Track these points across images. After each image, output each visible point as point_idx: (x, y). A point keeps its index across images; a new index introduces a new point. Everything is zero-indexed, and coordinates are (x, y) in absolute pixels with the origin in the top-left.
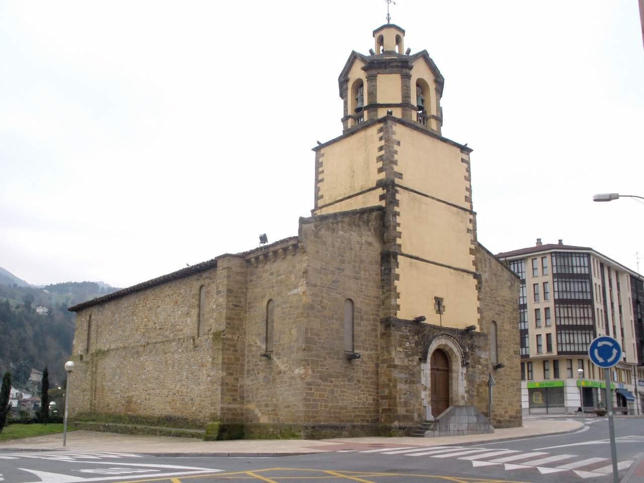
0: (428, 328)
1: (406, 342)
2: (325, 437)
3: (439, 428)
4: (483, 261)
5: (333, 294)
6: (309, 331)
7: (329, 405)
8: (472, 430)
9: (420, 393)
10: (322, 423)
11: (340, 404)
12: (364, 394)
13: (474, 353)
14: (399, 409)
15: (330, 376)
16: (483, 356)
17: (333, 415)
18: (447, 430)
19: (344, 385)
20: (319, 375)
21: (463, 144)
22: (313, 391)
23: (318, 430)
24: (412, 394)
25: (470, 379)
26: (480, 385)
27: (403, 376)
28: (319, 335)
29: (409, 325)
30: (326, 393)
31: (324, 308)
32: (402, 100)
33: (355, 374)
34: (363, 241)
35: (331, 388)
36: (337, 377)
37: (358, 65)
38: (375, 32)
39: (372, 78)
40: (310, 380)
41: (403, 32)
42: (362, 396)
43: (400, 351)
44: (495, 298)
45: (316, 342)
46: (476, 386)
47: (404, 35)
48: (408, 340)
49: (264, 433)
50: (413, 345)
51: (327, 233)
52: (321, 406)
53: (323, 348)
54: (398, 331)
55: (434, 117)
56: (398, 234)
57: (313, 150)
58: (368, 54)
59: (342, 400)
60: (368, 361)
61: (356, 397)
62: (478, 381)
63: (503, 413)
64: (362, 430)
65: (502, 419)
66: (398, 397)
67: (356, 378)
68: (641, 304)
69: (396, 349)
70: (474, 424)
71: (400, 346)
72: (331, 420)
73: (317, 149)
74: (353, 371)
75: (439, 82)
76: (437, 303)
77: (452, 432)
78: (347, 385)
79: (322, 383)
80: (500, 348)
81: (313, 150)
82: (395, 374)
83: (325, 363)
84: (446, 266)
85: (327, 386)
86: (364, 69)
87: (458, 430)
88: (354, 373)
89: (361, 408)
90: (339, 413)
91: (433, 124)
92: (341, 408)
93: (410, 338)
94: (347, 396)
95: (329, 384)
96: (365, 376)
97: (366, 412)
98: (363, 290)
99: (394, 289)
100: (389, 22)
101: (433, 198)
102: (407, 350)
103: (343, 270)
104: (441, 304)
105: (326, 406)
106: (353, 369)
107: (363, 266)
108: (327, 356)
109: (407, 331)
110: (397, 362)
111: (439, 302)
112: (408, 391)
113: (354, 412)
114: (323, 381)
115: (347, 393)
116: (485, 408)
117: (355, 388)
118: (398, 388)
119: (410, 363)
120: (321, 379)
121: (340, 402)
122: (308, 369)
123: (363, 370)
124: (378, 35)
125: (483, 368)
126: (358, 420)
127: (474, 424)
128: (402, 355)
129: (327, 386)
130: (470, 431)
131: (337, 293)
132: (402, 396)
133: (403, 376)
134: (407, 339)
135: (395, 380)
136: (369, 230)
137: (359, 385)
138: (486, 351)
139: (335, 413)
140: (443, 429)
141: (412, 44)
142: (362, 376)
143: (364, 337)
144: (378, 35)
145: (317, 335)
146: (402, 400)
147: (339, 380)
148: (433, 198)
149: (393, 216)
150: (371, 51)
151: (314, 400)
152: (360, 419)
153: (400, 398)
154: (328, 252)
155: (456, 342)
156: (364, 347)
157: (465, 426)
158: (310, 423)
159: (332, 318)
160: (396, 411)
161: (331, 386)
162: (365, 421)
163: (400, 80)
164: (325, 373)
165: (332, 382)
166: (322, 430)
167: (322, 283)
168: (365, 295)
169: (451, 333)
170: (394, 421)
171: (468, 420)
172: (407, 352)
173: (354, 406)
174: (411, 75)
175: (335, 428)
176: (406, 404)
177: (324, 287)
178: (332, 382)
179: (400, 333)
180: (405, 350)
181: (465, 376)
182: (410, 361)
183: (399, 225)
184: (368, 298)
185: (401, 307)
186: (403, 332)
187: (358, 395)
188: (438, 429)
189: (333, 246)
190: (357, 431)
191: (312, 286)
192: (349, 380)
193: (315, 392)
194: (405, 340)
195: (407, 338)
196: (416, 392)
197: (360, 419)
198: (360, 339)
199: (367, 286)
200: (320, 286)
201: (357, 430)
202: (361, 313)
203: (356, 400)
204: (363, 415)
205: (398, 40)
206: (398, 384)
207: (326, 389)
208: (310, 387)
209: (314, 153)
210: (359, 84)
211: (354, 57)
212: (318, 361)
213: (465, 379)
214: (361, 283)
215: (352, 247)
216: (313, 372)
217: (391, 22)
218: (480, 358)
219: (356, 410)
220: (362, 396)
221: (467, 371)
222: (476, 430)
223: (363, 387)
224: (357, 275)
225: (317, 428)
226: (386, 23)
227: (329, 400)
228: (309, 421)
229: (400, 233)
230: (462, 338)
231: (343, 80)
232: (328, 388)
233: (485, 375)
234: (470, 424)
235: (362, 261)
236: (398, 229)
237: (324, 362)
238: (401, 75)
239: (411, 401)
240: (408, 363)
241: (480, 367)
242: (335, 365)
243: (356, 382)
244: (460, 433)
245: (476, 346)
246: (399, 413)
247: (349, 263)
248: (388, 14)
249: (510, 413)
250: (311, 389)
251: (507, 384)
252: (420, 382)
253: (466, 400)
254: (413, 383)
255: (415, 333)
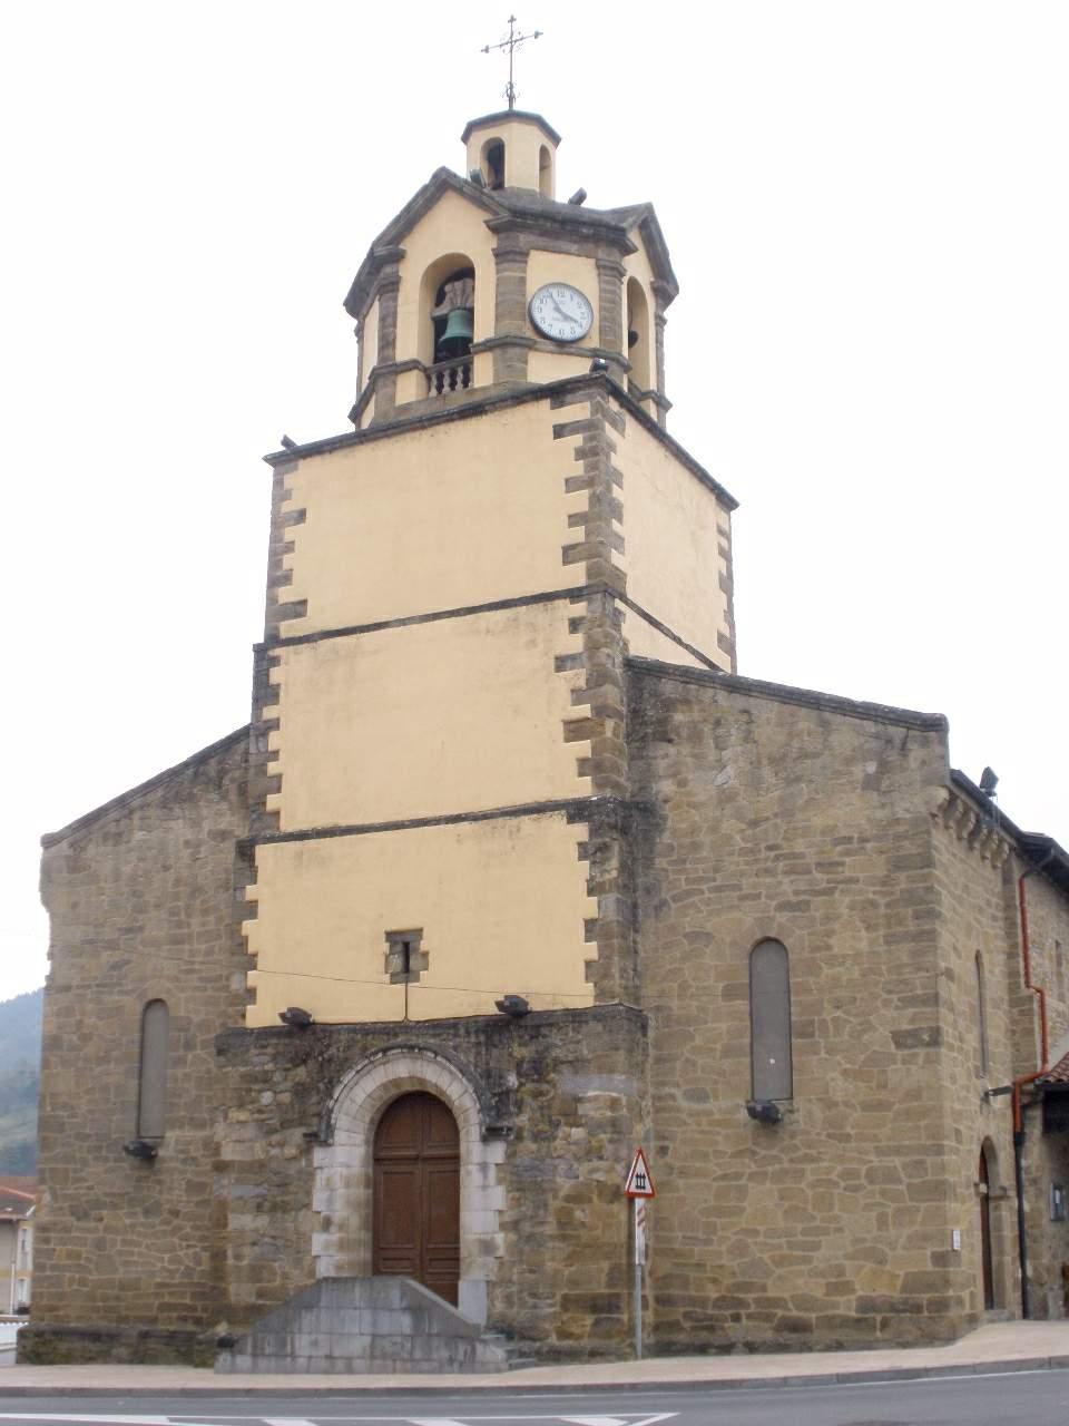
0: (342, 1037)
1: (260, 1091)
2: (68, 1359)
3: (255, 1347)
4: (707, 729)
5: (112, 999)
6: (48, 1101)
7: (90, 1277)
8: (380, 1355)
9: (309, 1241)
10: (72, 1325)
11: (120, 1274)
12: (188, 1247)
13: (545, 1087)
14: (232, 1288)
15: (98, 1204)
16: (591, 1094)
17: (101, 1304)
18: (280, 1355)
19: (132, 1226)
20: (71, 1206)
22: (52, 1246)
23: (50, 1341)
24: (280, 1242)
25: (524, 1183)
26: (576, 1198)
27: (249, 1191)
28: (72, 1108)
29: (274, 1041)
30: (83, 1249)
31: (85, 1038)
33: (165, 1196)
34: (204, 835)
35: (96, 1236)
36: (115, 1206)
40: (46, 1218)
42: (181, 1253)
43: (239, 1122)
44: (770, 848)
45: (63, 1124)
46: (554, 1204)
48: (267, 1086)
49: (794, 1334)
50: (286, 1098)
51: (102, 849)
52: (71, 1281)
53: (81, 1137)
54: (234, 1066)
59: (127, 1263)
60: (203, 1156)
61: (166, 1256)
62: (565, 1186)
63: (819, 1293)
64: (167, 1344)
65: (814, 1315)
66: (230, 1253)
67: (167, 1206)
68: (715, 772)
69: (226, 1117)
70: (399, 1339)
71: (241, 1106)
72: (94, 1316)
74: (158, 1188)
76: (399, 948)
77: (302, 1361)
78: (142, 1225)
79: (75, 1223)
80: (802, 1035)
82: (223, 1187)
83: (83, 1174)
84: (437, 821)
85: (89, 1231)
87: (329, 1357)
88: (161, 1192)
89: (180, 1285)
90: (118, 1298)
92: (123, 1286)
93: (277, 1077)
94: (140, 1254)
95: (92, 1224)
96: (196, 1199)
97: (194, 1295)
98: (197, 967)
99: (241, 945)
100: (511, 105)
101: (403, 622)
102: (263, 1116)
103: (141, 929)
104: (417, 949)
105: (83, 1282)
106: (160, 1182)
107: (198, 901)
108: (90, 1157)
109: (267, 1058)
110: (228, 1154)
111: (406, 946)
112: (263, 1235)
113: (157, 1295)
114: (79, 1219)
115: (139, 1245)
116: (604, 1278)
117: (164, 1231)
118: (231, 1227)
119: (274, 1152)
120: (72, 1214)
121: (121, 1270)
122: (44, 1192)
123: (189, 1182)
125: (591, 1134)
126: (170, 1318)
127: (399, 1339)
128: (249, 1132)
129: (89, 1231)
130: (378, 1362)
131: (122, 993)
132: (247, 1250)
133: (249, 1191)
134: (265, 1081)
135: (223, 1206)
136: (224, 798)
137: (176, 1222)
138: (611, 1071)
139: (105, 1299)
140: (268, 1350)
142: (184, 1199)
143: (194, 1093)
145: (65, 1106)
146: (245, 1262)
147: (121, 1212)
148: (403, 622)
149: (257, 737)
151: (53, 1268)
152: (175, 1315)
153: (238, 1257)
154: (103, 897)
155: (444, 1061)
156: (192, 1119)
157: (358, 1345)
158: (43, 1324)
159: (103, 1060)
160: (224, 1293)
161: (96, 1230)
162: (190, 1321)
163: (493, 265)
164: (84, 1199)
165: (101, 1219)
166: (61, 1340)
167: (83, 979)
168: (201, 979)
169: (434, 1036)
170: (217, 1323)
171: (374, 1323)
172: (263, 1120)
173: (159, 1280)
175: (95, 1336)
176: (256, 1272)
177: (89, 986)
178: (101, 1219)
179: (242, 1069)
180: (256, 1116)
181: (498, 1171)
182: (273, 1146)
183: (275, 755)
184: (209, 985)
185: (260, 995)
186: (252, 1064)
187: (173, 1249)
188: (249, 1349)
189: (117, 876)
190: (153, 1346)
191: (57, 992)
192: (147, 1212)
193: (58, 1248)
194: (256, 1087)
195: (265, 1079)
196: (294, 1238)
197: (175, 1315)
198: (183, 1101)
199: (209, 952)
200: (78, 987)
201: (152, 1344)
202: (188, 1030)
203: (166, 1264)
204: (186, 1305)
206: (230, 1216)
207: (86, 1239)
208: (46, 1235)
212: (66, 1171)
213: (500, 1181)
214: (191, 951)
215: (171, 861)
216: (55, 1197)
217: (518, 107)
218: (578, 1100)
219: (165, 1290)
220: (181, 1253)
221: (510, 1155)
222: (412, 1360)
223: (188, 1230)
224: (178, 931)
225: (47, 1337)
227: (91, 1266)
228: (42, 1320)
229: (279, 777)
230: (490, 1044)
232: (90, 1236)
233: (601, 1158)
234: (383, 1336)
235: (196, 890)
236: (273, 768)
237: (82, 1171)
239: (276, 1265)
240: (267, 1152)
241: (578, 1133)
242: (108, 1175)
243: (166, 1215)
244: (331, 1364)
245: (558, 1063)
246: (233, 1299)
247: (157, 906)
249: (860, 1293)
250: (47, 1241)
251: (847, 1174)
252: (308, 1206)
253: (501, 1252)
254: (284, 1212)
255: (292, 1060)
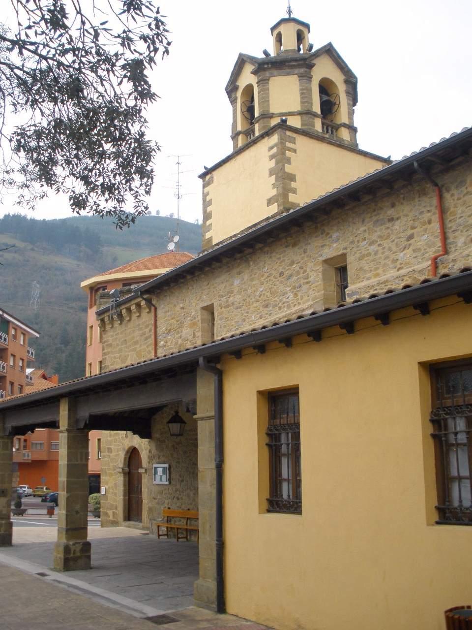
21: (386, 157)
32: (301, 108)
37: (249, 68)
38: (273, 29)
39: (263, 82)
41: (307, 26)
47: (309, 32)
55: (344, 125)
56: (66, 342)
57: (200, 177)
58: (261, 56)
73: (202, 176)
75: (351, 82)
81: (200, 177)
86: (254, 73)
91: (345, 134)
124: (276, 32)
141: (316, 40)
144: (276, 32)
150: (266, 53)
163: (298, 83)
174: (238, 86)
205: (300, 37)
209: (201, 181)
210: (249, 89)
211: (242, 61)
217: (292, 16)
226: (287, 17)
231: (231, 89)
238: (299, 77)
248: (289, 8)
